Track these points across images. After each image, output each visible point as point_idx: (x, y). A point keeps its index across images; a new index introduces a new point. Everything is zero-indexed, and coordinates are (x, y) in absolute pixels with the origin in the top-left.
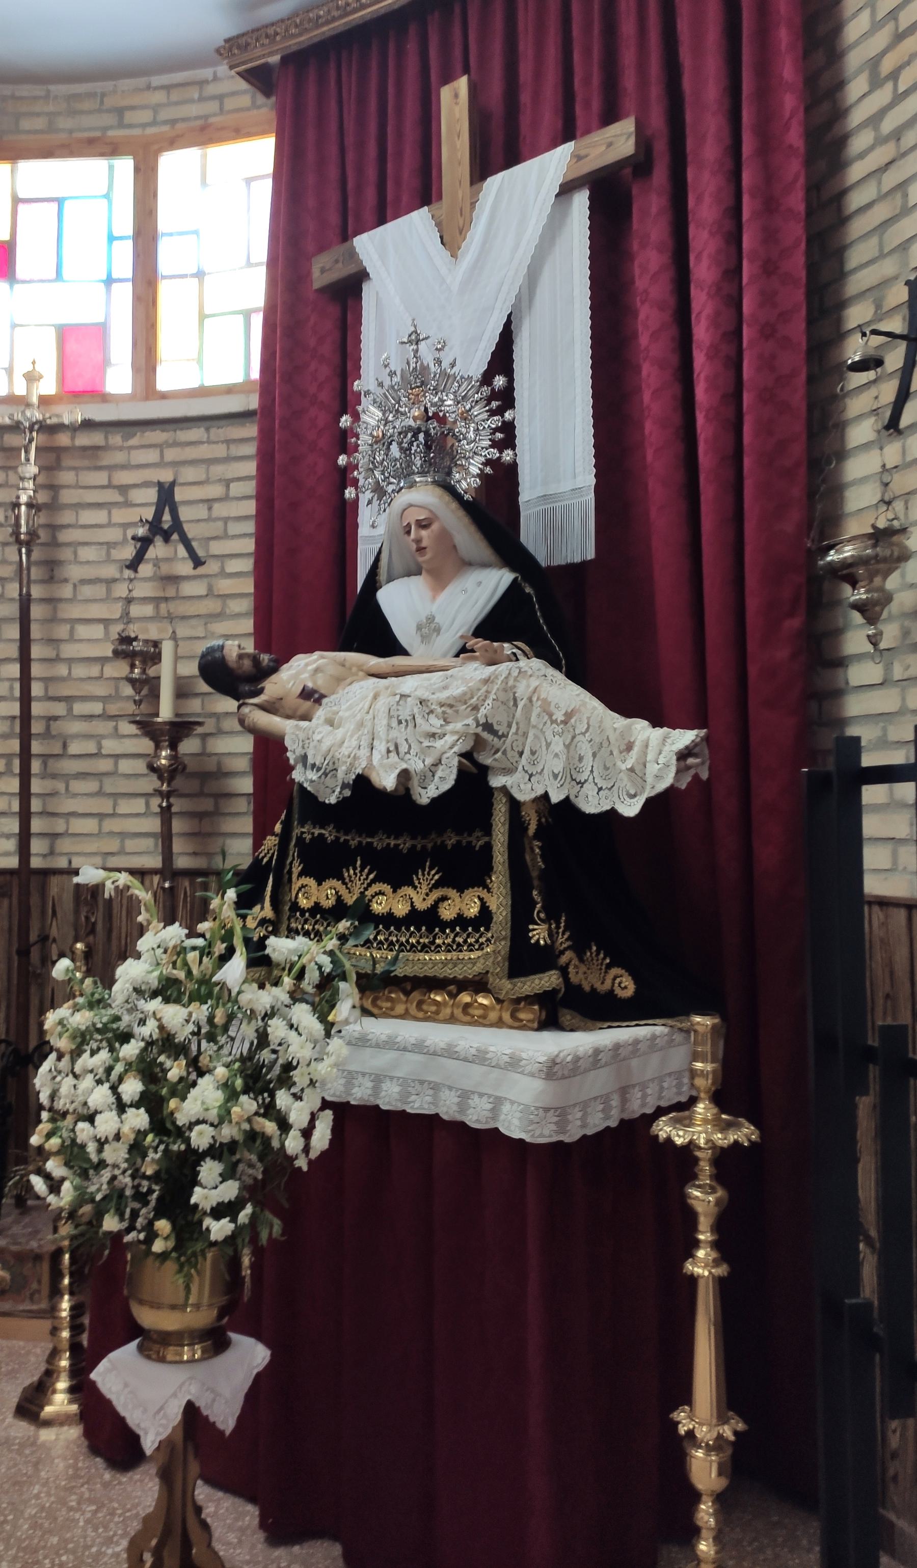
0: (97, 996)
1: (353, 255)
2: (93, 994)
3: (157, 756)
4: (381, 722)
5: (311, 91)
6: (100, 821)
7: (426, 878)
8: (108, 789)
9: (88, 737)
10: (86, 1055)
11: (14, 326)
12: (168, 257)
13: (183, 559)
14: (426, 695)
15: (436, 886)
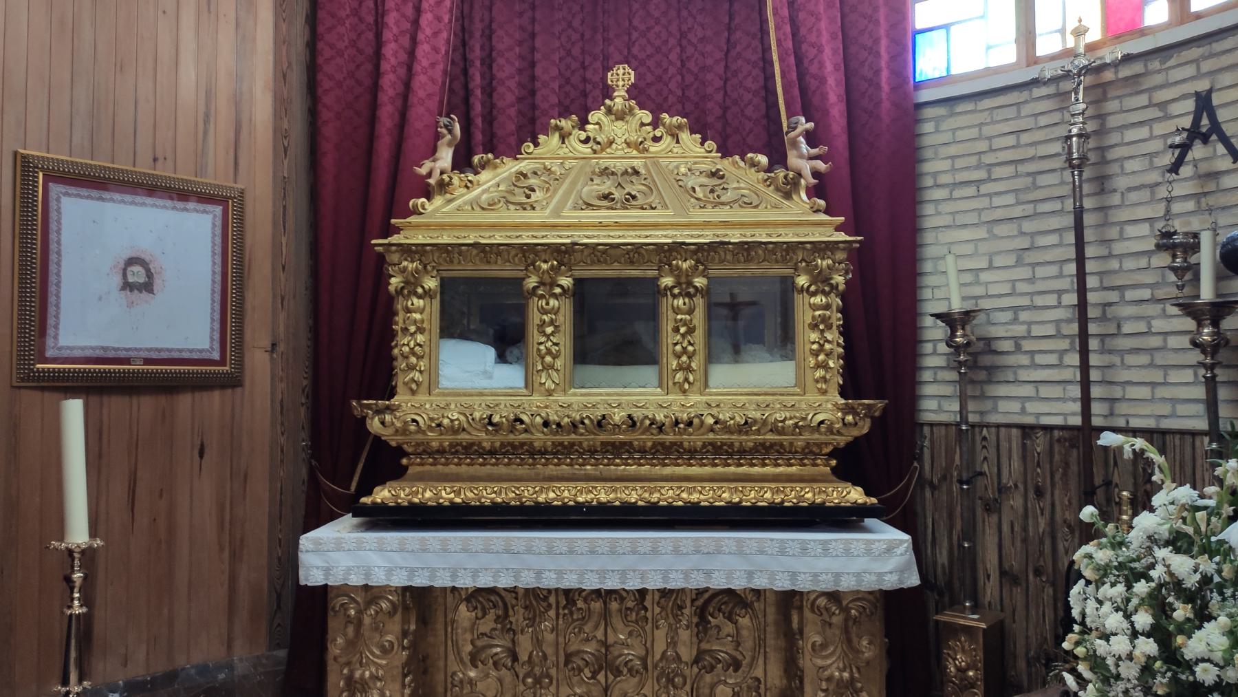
0: (1118, 539)
2: (1114, 537)
3: (1199, 333)
6: (1153, 388)
8: (1159, 361)
9: (1139, 318)
10: (1107, 586)
11: (989, 48)
13: (1223, 155)
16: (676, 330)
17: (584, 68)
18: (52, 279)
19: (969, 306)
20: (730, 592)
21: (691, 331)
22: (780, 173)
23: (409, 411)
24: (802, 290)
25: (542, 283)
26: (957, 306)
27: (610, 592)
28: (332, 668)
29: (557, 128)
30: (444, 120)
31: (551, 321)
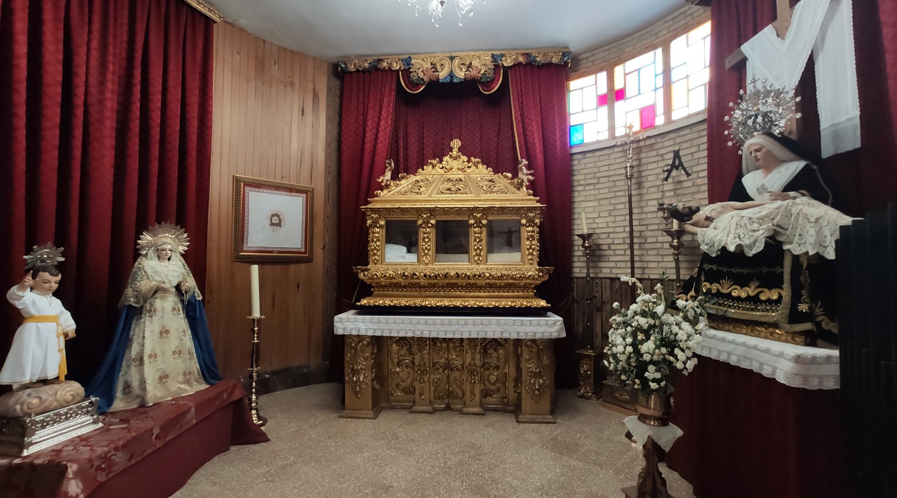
1: (741, 52)
4: (734, 227)
5: (518, 73)
7: (753, 285)
12: (674, 75)
14: (751, 216)
15: (758, 287)
16: (475, 240)
17: (443, 139)
18: (246, 222)
19: (590, 232)
20: (495, 340)
21: (481, 241)
22: (516, 180)
23: (374, 270)
24: (523, 225)
25: (424, 223)
26: (585, 231)
27: (450, 339)
28: (346, 365)
29: (431, 163)
30: (388, 161)
31: (428, 237)
